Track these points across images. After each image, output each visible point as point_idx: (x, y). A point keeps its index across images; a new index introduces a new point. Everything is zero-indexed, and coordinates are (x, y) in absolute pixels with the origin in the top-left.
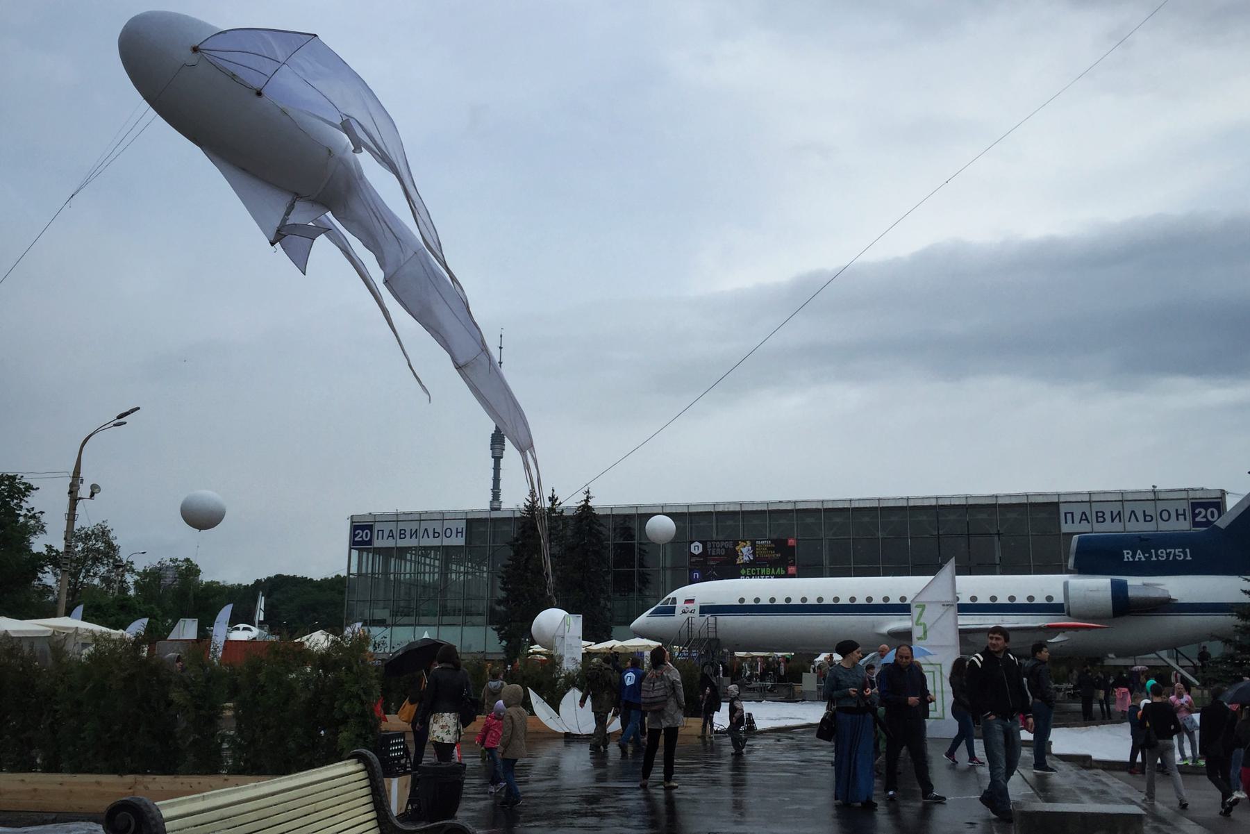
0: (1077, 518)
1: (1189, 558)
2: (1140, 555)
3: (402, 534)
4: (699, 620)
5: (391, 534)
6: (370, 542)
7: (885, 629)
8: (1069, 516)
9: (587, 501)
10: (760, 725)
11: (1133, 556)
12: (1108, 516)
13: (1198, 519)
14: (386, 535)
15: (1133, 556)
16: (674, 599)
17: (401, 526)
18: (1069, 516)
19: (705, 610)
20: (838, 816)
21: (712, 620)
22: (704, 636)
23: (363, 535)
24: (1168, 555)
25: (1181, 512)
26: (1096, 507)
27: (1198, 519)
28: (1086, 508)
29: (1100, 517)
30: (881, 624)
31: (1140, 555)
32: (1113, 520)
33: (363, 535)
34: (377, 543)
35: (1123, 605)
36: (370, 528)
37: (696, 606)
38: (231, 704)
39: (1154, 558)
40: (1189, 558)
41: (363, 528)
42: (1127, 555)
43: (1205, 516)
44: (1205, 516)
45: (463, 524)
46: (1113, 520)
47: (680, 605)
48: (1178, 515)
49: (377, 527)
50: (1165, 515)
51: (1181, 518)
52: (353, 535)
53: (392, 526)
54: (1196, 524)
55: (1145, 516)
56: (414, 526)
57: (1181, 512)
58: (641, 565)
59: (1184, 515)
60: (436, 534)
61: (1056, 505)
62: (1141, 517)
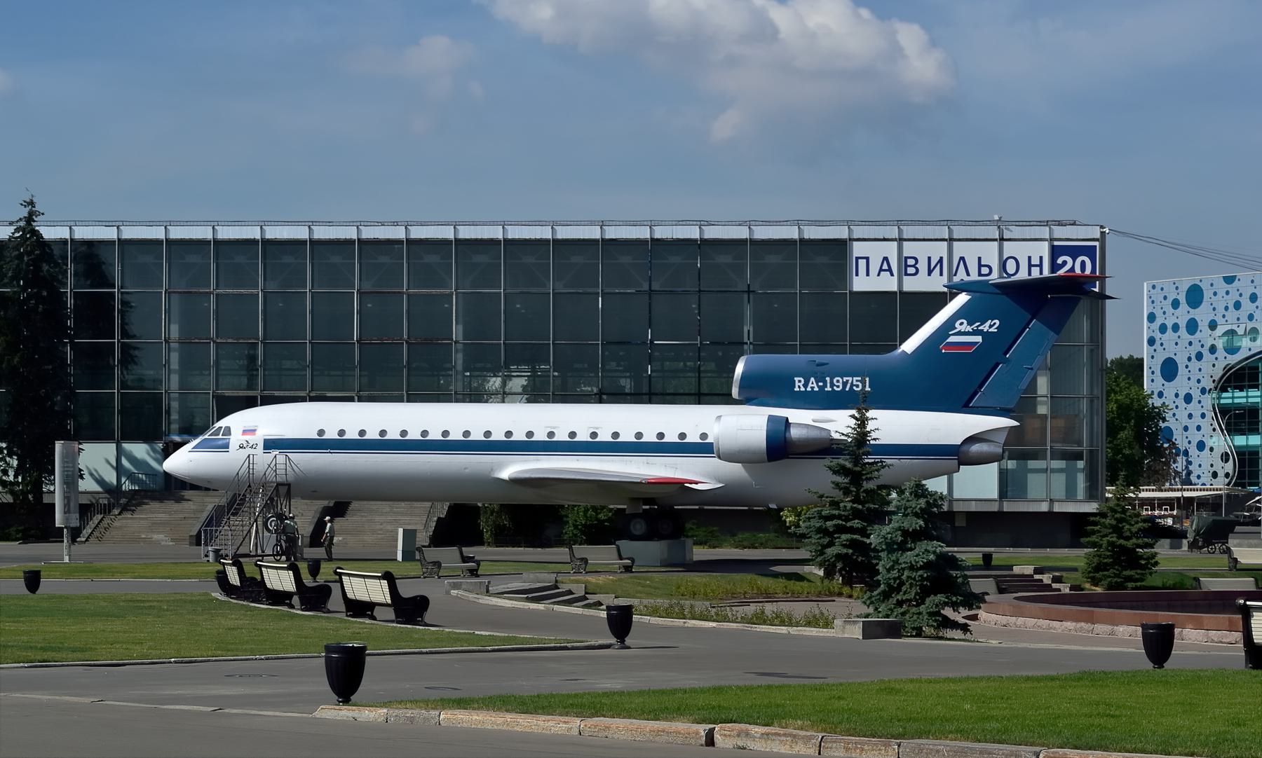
1: (868, 389)
2: (813, 385)
4: (263, 460)
7: (505, 474)
8: (862, 263)
11: (805, 385)
12: (923, 266)
14: (874, 268)
15: (805, 385)
16: (228, 431)
18: (862, 263)
19: (270, 445)
21: (281, 459)
22: (270, 476)
24: (845, 384)
25: (1035, 261)
30: (501, 466)
31: (813, 385)
32: (930, 272)
35: (780, 446)
37: (258, 438)
39: (828, 389)
40: (868, 389)
41: (1074, 252)
42: (799, 384)
43: (1072, 269)
44: (1072, 269)
46: (930, 272)
47: (236, 438)
55: (980, 266)
58: (125, 334)
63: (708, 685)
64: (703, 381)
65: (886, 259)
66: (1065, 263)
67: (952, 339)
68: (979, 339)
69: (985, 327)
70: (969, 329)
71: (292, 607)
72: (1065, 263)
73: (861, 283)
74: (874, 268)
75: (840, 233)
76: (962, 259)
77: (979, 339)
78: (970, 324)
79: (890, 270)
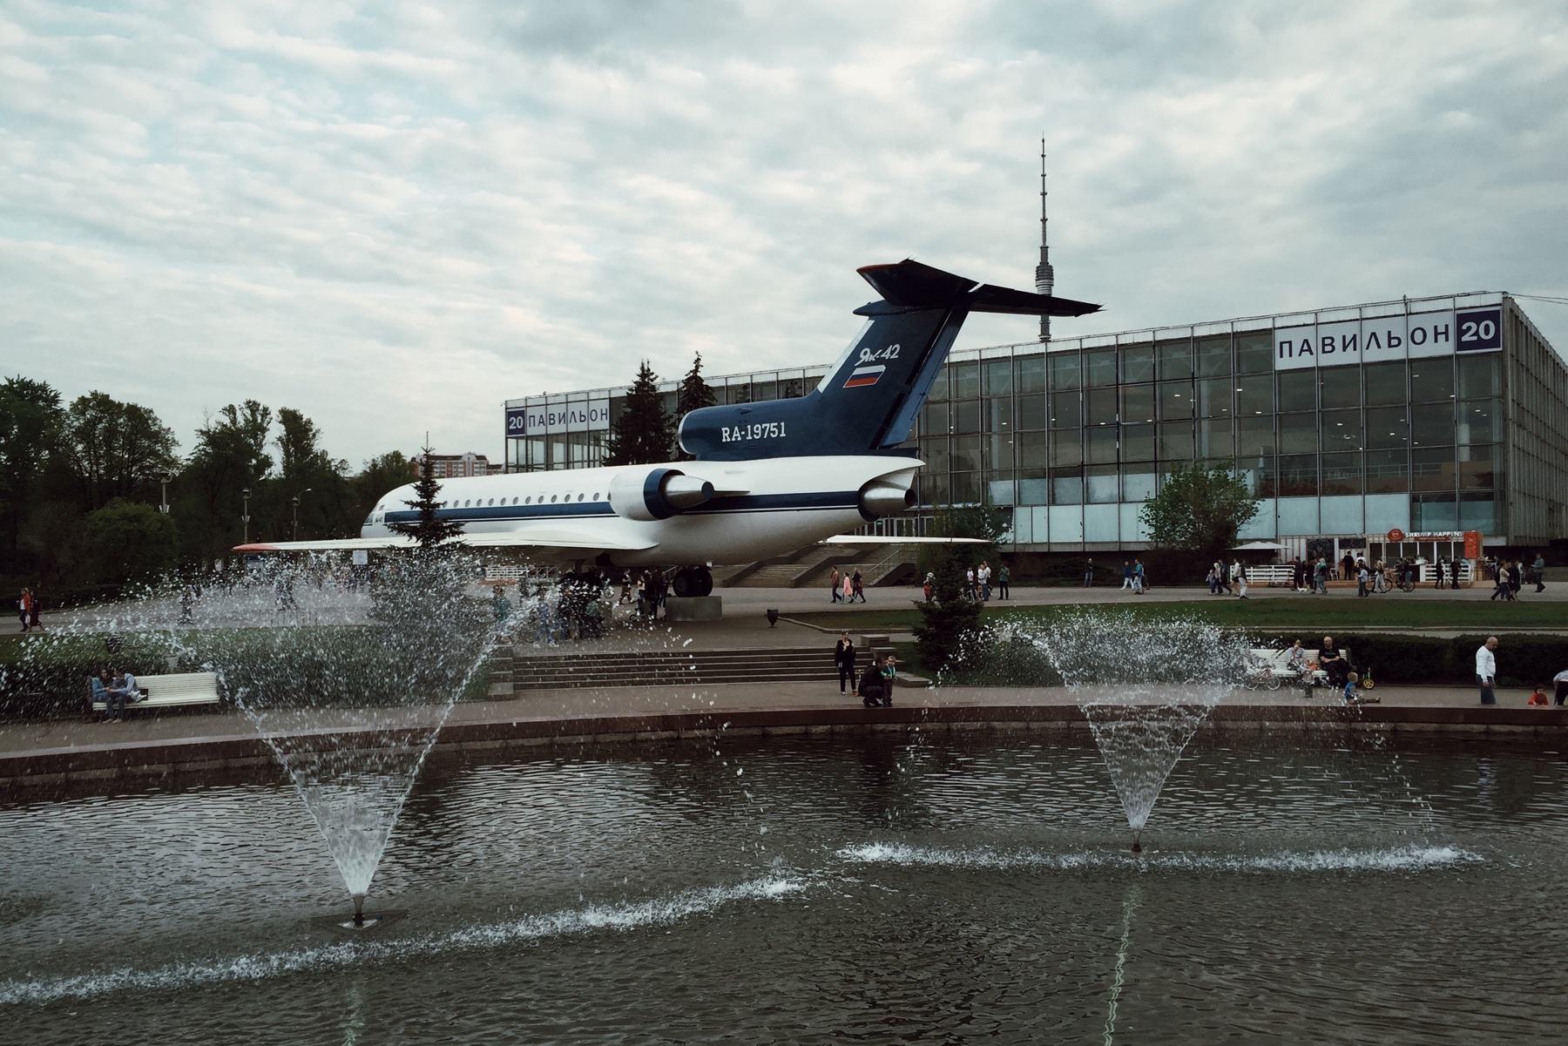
0: (1296, 349)
3: (1327, 345)
5: (1306, 347)
6: (522, 430)
8: (1286, 347)
9: (696, 370)
10: (727, 609)
12: (1338, 344)
13: (1465, 338)
14: (1296, 350)
17: (1325, 331)
18: (1286, 347)
20: (967, 685)
23: (517, 422)
24: (763, 430)
25: (1441, 329)
26: (1369, 327)
27: (1465, 338)
28: (1309, 334)
29: (1327, 345)
33: (517, 422)
34: (531, 431)
36: (522, 413)
38: (970, 574)
41: (1478, 317)
43: (1477, 333)
44: (1477, 333)
45: (605, 405)
48: (1436, 334)
49: (530, 412)
50: (1419, 336)
51: (1441, 338)
52: (508, 423)
53: (1309, 334)
54: (1461, 345)
55: (1390, 338)
56: (1350, 330)
57: (1441, 329)
59: (1446, 333)
60: (583, 418)
61: (1268, 333)
62: (1384, 341)
63: (58, 818)
64: (1130, 459)
65: (1306, 341)
66: (1469, 328)
67: (858, 372)
68: (882, 368)
69: (887, 355)
70: (872, 358)
71: (280, 742)
72: (1469, 328)
73: (1282, 364)
74: (1296, 350)
75: (1268, 324)
76: (1374, 334)
77: (882, 368)
78: (873, 353)
79: (1310, 350)
